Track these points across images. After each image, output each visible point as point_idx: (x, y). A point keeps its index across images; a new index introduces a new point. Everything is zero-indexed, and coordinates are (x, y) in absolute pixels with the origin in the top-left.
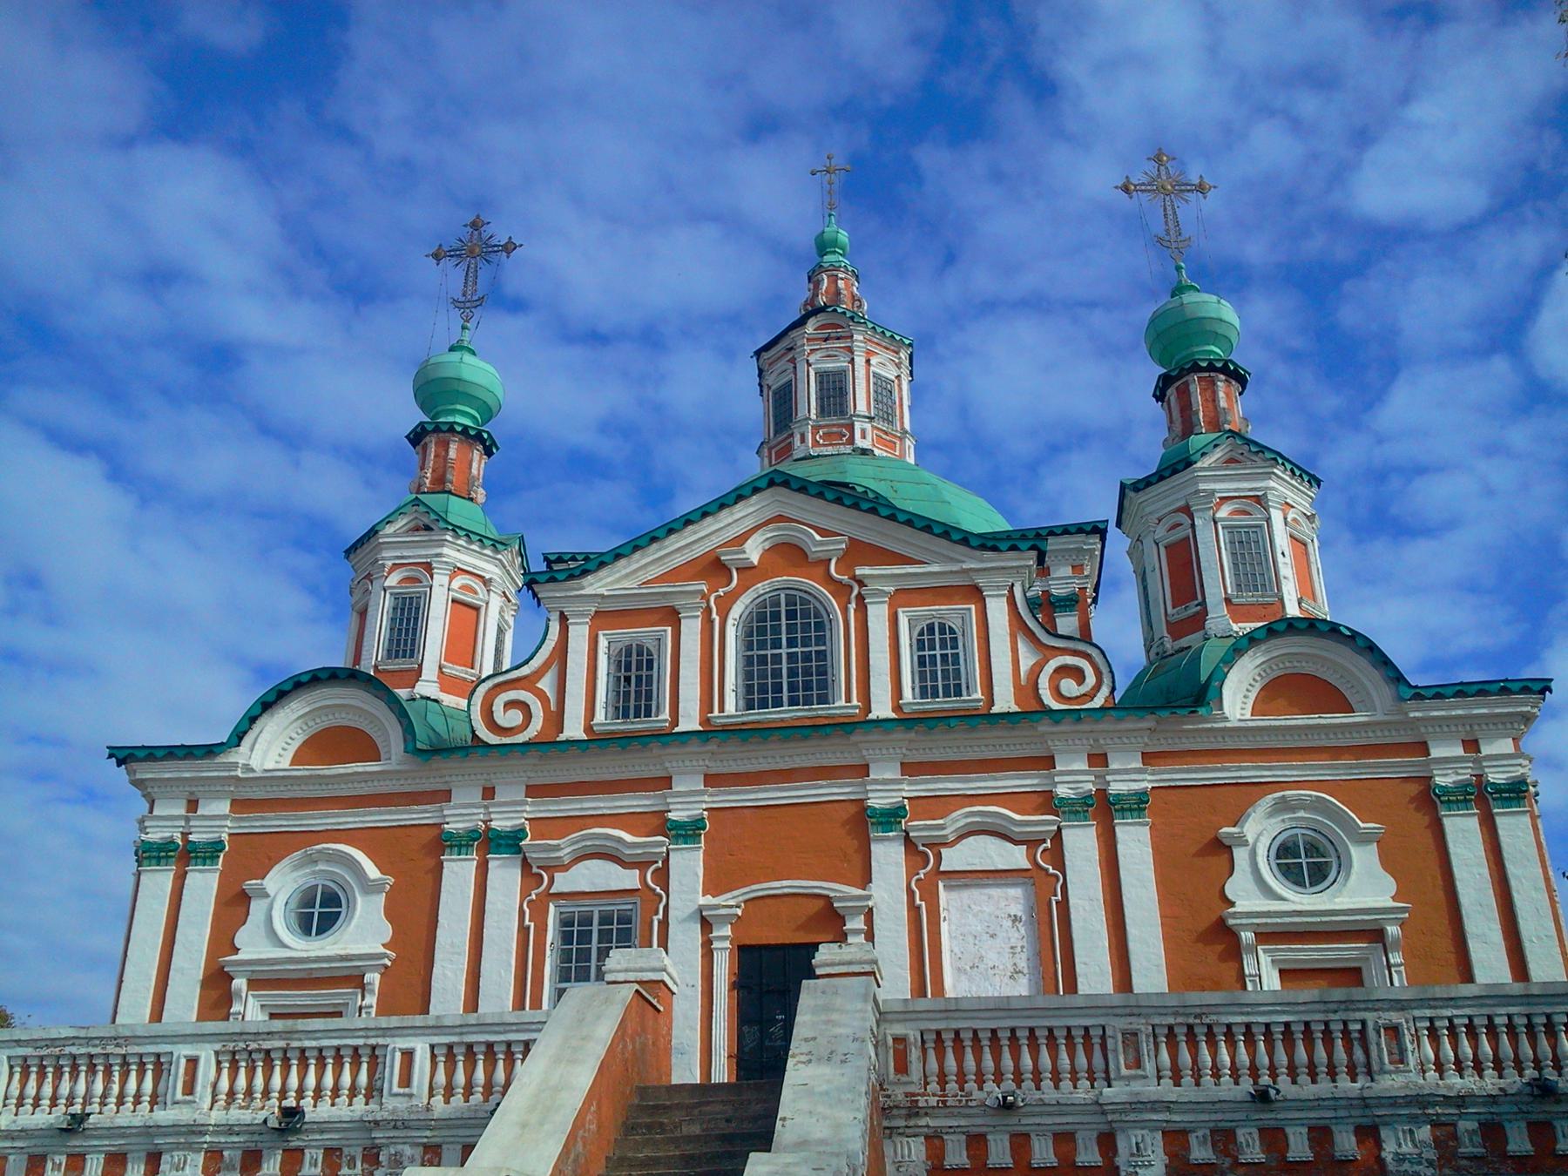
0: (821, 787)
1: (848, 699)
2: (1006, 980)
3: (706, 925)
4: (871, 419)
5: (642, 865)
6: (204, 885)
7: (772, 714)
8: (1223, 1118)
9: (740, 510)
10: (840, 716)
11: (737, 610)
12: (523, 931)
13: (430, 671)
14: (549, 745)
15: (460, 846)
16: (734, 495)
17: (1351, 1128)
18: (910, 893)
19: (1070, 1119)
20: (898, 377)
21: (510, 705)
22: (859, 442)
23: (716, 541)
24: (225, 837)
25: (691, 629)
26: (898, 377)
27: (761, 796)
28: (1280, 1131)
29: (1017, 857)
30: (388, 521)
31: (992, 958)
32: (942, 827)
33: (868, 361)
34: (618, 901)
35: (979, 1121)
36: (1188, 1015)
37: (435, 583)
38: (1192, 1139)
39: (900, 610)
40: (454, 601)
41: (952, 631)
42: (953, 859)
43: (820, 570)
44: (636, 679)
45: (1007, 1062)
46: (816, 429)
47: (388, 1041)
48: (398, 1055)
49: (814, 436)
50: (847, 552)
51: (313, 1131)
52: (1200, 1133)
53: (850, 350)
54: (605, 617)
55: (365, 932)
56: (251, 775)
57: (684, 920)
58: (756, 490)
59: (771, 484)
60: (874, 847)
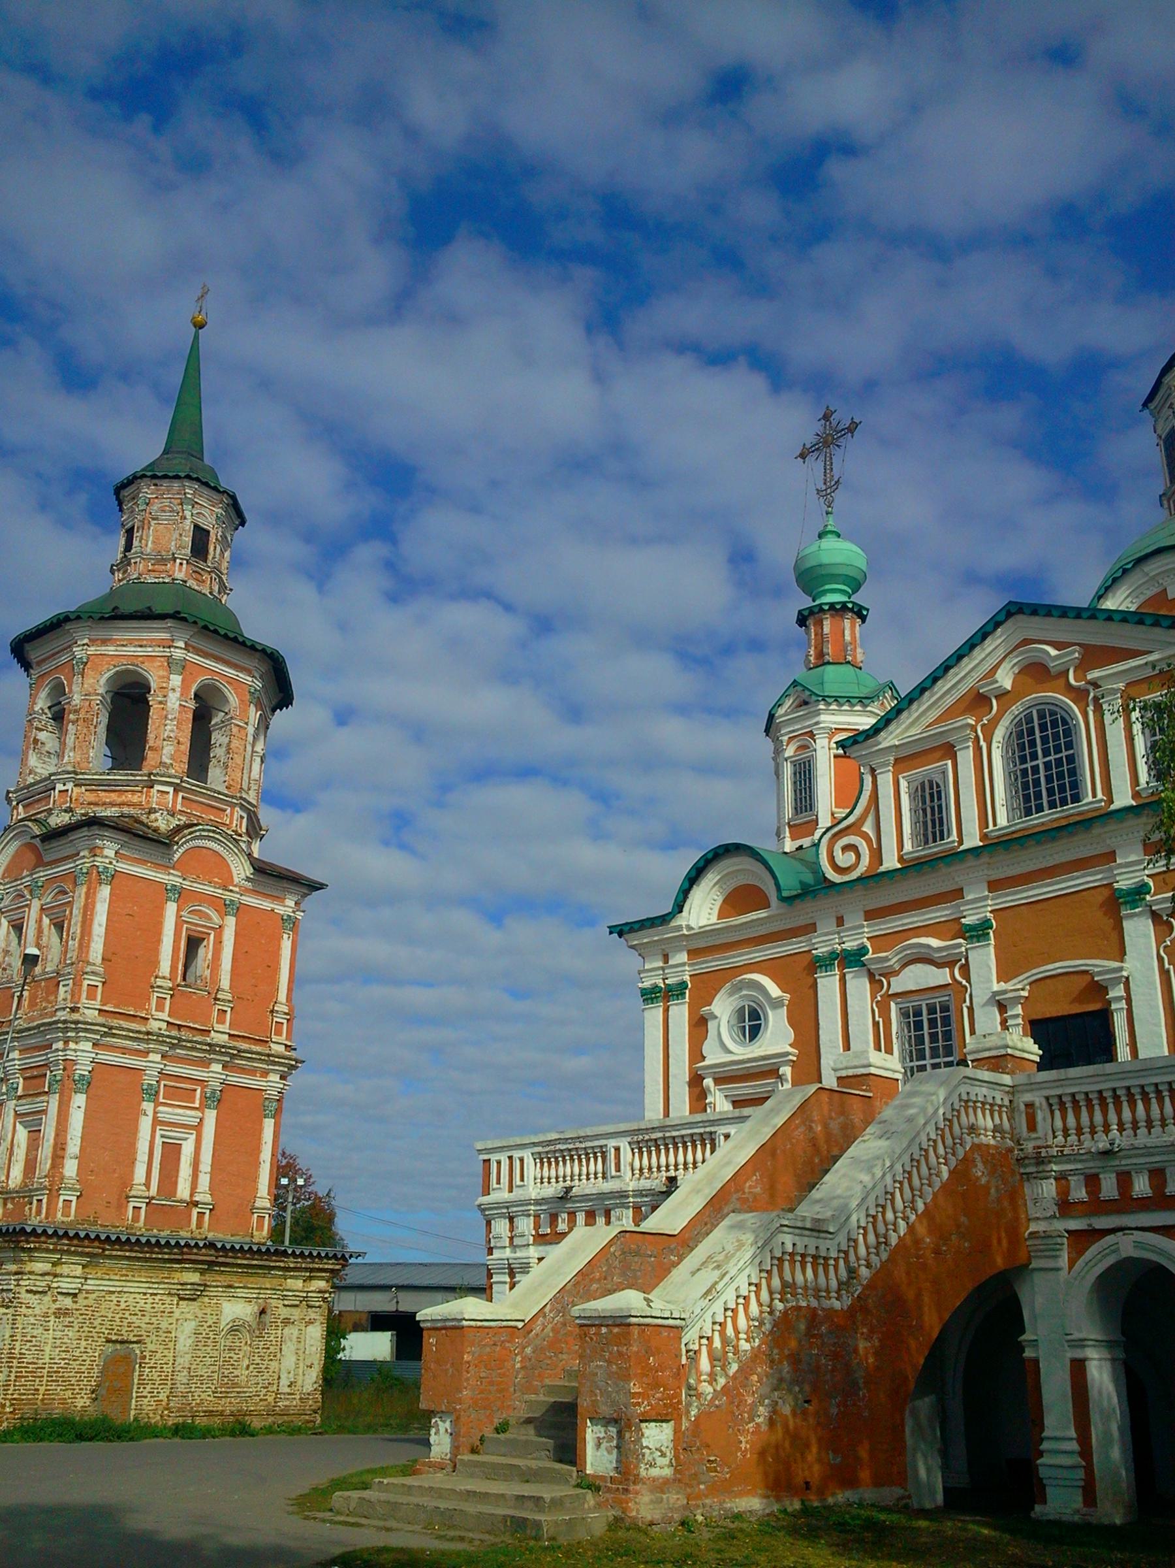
0: (1078, 878)
1: (1094, 795)
3: (1002, 1007)
5: (951, 964)
6: (680, 1012)
9: (990, 644)
10: (1088, 811)
11: (999, 734)
12: (876, 1024)
13: (825, 821)
14: (875, 878)
15: (826, 966)
19: (1158, 1158)
21: (846, 848)
24: (687, 978)
25: (966, 757)
27: (1031, 893)
30: (779, 705)
34: (937, 995)
35: (1091, 1164)
37: (818, 747)
44: (932, 807)
45: (1113, 1117)
54: (905, 760)
55: (778, 1038)
57: (984, 1005)
58: (998, 625)
59: (1009, 615)
60: (1125, 924)
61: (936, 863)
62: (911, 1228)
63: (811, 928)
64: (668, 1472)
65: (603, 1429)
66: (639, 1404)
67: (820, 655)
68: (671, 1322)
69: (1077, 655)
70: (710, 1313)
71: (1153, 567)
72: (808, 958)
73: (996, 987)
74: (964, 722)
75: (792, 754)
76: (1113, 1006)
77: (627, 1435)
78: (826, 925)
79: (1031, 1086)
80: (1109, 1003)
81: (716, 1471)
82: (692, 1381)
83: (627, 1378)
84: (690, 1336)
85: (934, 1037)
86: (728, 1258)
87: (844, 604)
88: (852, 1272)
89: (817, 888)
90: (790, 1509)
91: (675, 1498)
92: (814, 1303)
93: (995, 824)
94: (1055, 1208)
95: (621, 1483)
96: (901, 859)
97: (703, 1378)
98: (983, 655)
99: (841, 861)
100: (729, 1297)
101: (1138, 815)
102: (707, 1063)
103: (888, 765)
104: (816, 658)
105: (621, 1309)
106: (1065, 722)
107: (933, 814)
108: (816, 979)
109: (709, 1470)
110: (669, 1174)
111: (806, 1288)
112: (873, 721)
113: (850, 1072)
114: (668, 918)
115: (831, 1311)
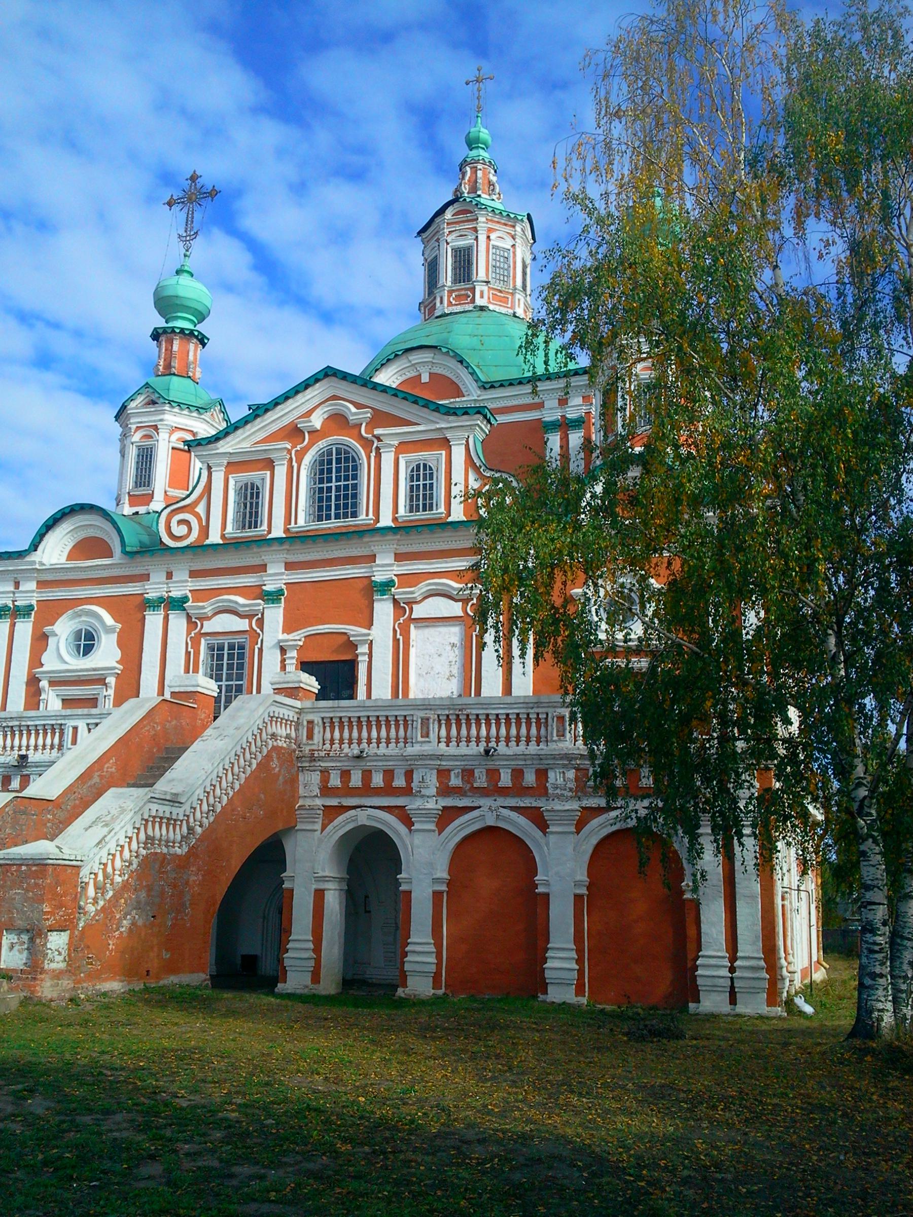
1: (367, 515)
2: (445, 680)
3: (283, 651)
4: (487, 282)
5: (250, 617)
6: (25, 629)
7: (325, 525)
8: (468, 764)
10: (362, 525)
11: (308, 459)
12: (188, 653)
13: (159, 496)
14: (200, 548)
15: (154, 607)
16: (294, 391)
17: (534, 770)
18: (395, 631)
19: (391, 763)
20: (513, 246)
21: (180, 522)
22: (479, 302)
23: (297, 413)
24: (34, 603)
25: (281, 471)
26: (513, 246)
28: (497, 771)
29: (456, 609)
31: (438, 668)
32: (412, 593)
33: (488, 237)
35: (346, 764)
36: (456, 709)
38: (452, 773)
39: (400, 456)
40: (173, 448)
41: (431, 469)
42: (419, 611)
43: (356, 431)
44: (251, 503)
46: (450, 292)
47: (66, 721)
48: (71, 729)
49: (449, 297)
50: (372, 419)
51: (33, 767)
52: (456, 771)
53: (475, 230)
54: (234, 466)
55: (107, 655)
56: (44, 567)
58: (317, 381)
59: (326, 375)
61: (247, 545)
62: (230, 801)
63: (145, 577)
64: (62, 966)
65: (16, 937)
66: (48, 919)
67: (168, 366)
68: (74, 863)
69: (369, 415)
70: (98, 857)
71: (415, 357)
72: (140, 599)
73: (282, 636)
74: (283, 446)
75: (138, 440)
76: (360, 658)
77: (38, 941)
78: (157, 577)
79: (313, 710)
80: (357, 656)
81: (92, 964)
82: (82, 903)
83: (41, 901)
84: (84, 872)
85: (230, 667)
86: (114, 819)
87: (192, 331)
88: (191, 829)
89: (152, 548)
90: (137, 989)
91: (66, 983)
92: (165, 850)
93: (296, 523)
94: (318, 791)
95: (30, 974)
96: (223, 536)
97: (89, 901)
98: (303, 400)
99: (178, 531)
100: (112, 846)
101: (395, 534)
102: (44, 669)
103: (222, 466)
104: (164, 368)
105: (41, 854)
106: (354, 460)
107: (251, 508)
108: (144, 616)
109: (88, 963)
110: (21, 753)
111: (160, 840)
112: (214, 433)
113: (182, 689)
114: (23, 554)
115: (175, 855)
